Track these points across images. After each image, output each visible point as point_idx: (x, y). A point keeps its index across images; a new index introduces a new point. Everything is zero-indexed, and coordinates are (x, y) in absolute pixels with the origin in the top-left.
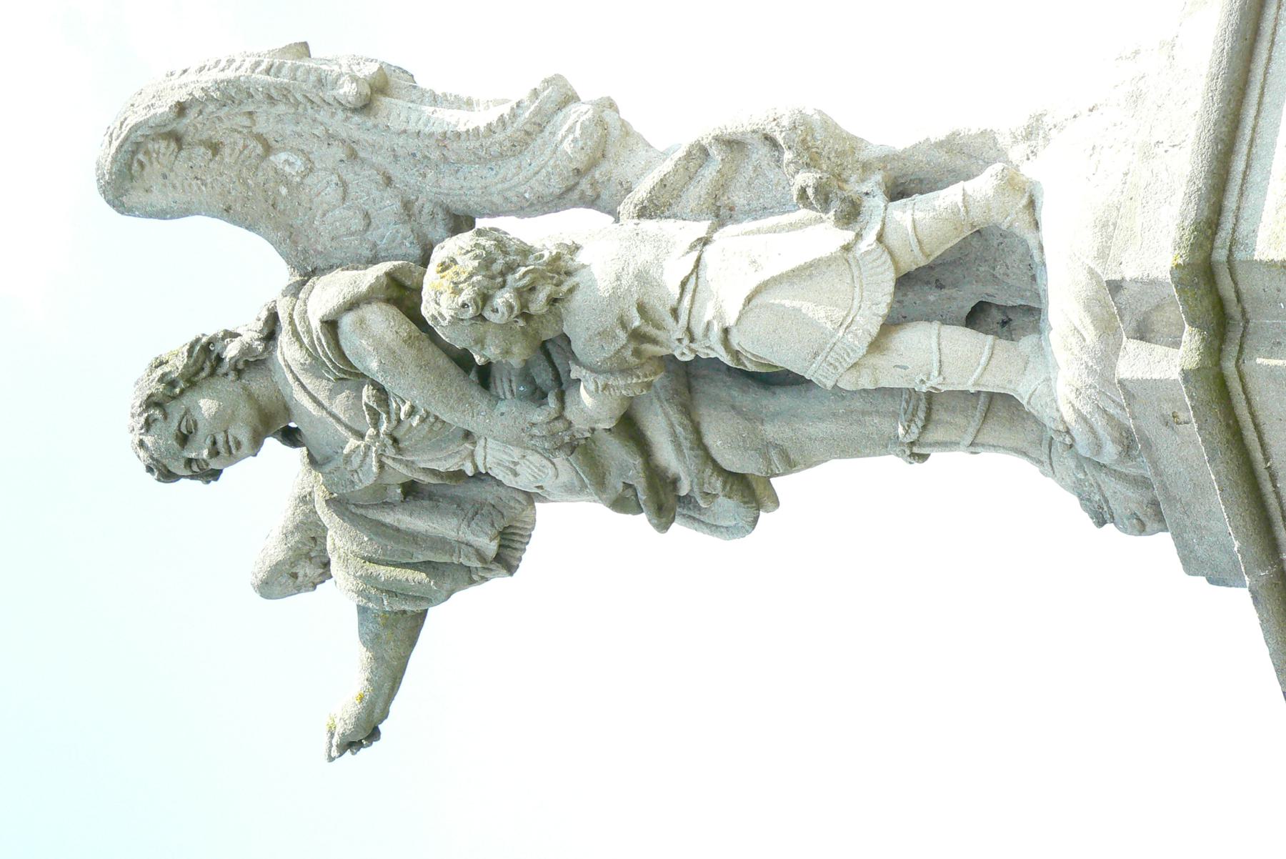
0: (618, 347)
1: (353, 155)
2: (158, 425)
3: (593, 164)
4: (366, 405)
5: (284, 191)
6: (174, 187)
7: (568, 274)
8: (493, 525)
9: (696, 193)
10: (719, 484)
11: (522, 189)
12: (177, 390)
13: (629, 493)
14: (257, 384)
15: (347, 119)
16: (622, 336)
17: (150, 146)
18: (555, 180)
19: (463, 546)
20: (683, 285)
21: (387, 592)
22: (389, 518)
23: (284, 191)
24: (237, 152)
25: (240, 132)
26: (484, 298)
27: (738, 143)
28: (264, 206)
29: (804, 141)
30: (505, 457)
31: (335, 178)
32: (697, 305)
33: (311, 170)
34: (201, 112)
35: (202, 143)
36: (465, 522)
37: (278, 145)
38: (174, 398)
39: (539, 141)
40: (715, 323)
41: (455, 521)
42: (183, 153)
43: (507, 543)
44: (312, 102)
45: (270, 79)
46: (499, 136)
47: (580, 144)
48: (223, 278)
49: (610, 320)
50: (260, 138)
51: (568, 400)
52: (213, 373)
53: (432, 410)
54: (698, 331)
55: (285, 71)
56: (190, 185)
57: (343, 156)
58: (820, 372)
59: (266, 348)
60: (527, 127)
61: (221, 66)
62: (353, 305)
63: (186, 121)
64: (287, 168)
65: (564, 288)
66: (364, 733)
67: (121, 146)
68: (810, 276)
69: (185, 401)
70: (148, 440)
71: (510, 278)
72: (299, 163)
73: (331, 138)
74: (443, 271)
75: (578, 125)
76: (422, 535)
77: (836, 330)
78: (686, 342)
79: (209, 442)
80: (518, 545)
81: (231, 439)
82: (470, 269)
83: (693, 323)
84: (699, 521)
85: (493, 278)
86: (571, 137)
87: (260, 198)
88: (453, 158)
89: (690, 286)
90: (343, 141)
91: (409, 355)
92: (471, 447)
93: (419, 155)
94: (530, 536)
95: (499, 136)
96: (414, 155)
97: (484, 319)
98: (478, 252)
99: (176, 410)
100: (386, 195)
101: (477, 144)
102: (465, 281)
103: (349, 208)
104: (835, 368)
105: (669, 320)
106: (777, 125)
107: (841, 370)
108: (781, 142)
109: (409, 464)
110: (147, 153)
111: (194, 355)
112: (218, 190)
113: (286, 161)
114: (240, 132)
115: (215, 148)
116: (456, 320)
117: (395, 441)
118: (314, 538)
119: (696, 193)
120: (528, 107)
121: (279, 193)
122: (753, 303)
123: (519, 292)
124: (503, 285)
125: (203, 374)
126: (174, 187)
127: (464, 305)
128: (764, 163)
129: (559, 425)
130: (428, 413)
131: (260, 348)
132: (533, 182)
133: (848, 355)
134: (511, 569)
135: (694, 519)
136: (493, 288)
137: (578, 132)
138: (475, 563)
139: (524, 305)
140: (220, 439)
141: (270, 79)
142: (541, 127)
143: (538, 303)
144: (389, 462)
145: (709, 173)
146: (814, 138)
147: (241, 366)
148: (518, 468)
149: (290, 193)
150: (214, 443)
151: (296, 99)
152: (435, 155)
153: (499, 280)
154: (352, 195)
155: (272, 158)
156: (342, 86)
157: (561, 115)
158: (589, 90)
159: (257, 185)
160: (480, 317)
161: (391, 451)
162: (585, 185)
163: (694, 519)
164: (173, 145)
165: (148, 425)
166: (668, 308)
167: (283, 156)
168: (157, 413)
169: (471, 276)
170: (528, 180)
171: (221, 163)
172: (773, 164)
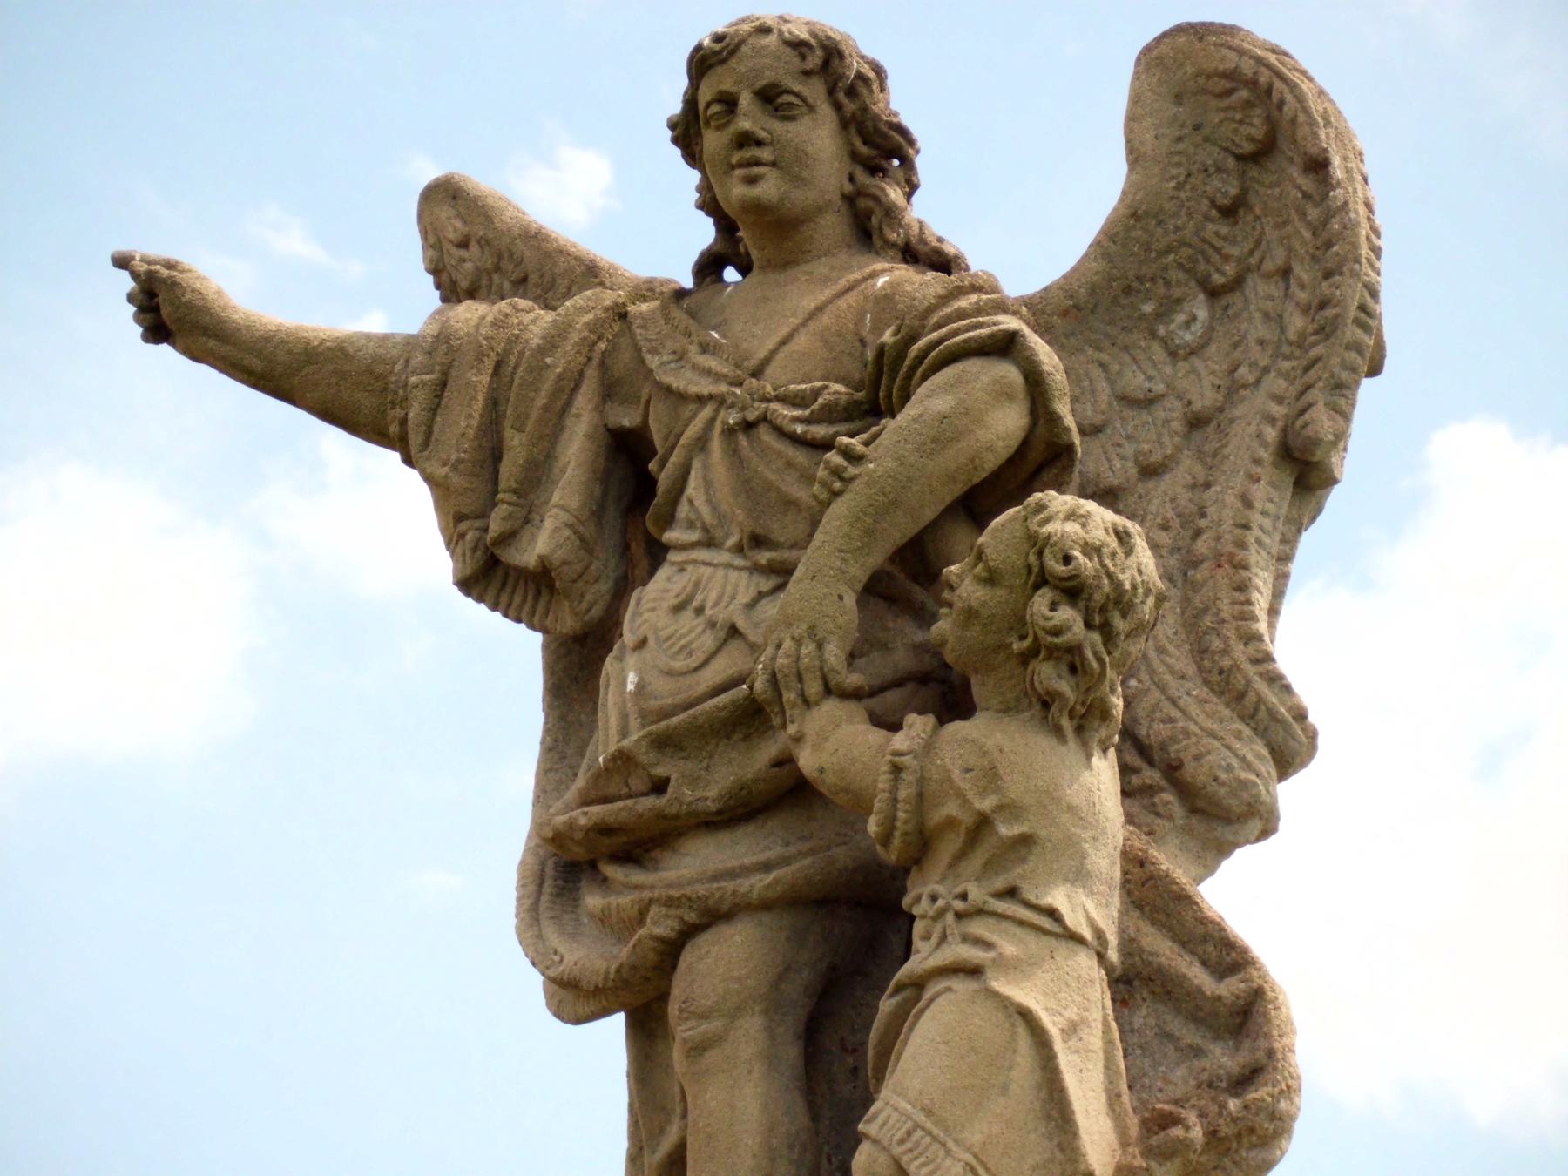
0: (970, 795)
1: (1196, 422)
2: (796, 60)
3: (1186, 792)
4: (826, 387)
5: (1148, 308)
6: (1179, 139)
7: (1079, 730)
8: (564, 563)
9: (1161, 948)
10: (659, 931)
11: (1144, 676)
12: (841, 96)
13: (637, 784)
14: (833, 225)
15: (1272, 420)
16: (986, 804)
17: (1258, 111)
18: (1163, 730)
19: (524, 512)
20: (1052, 913)
21: (443, 385)
22: (584, 402)
23: (1148, 308)
24: (1218, 243)
25: (1251, 252)
26: (1072, 591)
27: (1242, 1025)
28: (1131, 274)
29: (1252, 1130)
30: (713, 595)
31: (1160, 388)
32: (1018, 931)
33: (1173, 354)
34: (1306, 196)
35: (1244, 192)
36: (572, 520)
37: (1219, 312)
38: (831, 92)
39: (1227, 712)
40: (991, 954)
41: (574, 503)
42: (1231, 162)
43: (511, 581)
44: (1307, 369)
45: (1352, 311)
46: (1239, 651)
47: (1223, 776)
48: (1021, 188)
49: (1015, 788)
50: (1237, 283)
51: (852, 706)
52: (854, 156)
53: (856, 485)
54: (978, 927)
55: (1359, 333)
56: (1178, 165)
57: (1197, 406)
58: (895, 1116)
59: (894, 245)
60: (1251, 698)
61: (1373, 237)
62: (1035, 382)
63: (1295, 172)
64: (1181, 318)
65: (1065, 723)
66: (168, 310)
67: (1268, 66)
68: (1048, 1117)
69: (825, 110)
70: (771, 40)
71: (1096, 637)
72: (1188, 337)
73: (1233, 390)
74: (1117, 533)
75: (1253, 777)
76: (545, 443)
77: (968, 1149)
78: (959, 905)
79: (762, 134)
80: (504, 598)
81: (762, 170)
82: (1121, 577)
83: (992, 921)
84: (539, 893)
85: (1103, 610)
86: (1235, 762)
87: (1144, 270)
88: (1198, 575)
89: (1046, 923)
90: (1221, 410)
91: (950, 459)
92: (731, 542)
93: (1203, 523)
94: (518, 620)
95: (1239, 651)
96: (1203, 515)
97: (1036, 587)
98: (1140, 591)
99: (815, 90)
100: (1130, 464)
101: (1225, 615)
102: (1104, 566)
103: (1110, 404)
104: (902, 1141)
105: (1000, 883)
106: (1282, 1091)
107: (897, 1150)
108: (1251, 1096)
109: (702, 443)
110: (1248, 104)
111: (892, 133)
112: (1167, 206)
113: (1194, 318)
114: (1251, 252)
115: (1229, 212)
116: (1039, 544)
117: (748, 426)
118: (524, 280)
119: (1161, 948)
120: (1283, 703)
121: (1148, 299)
122: (1019, 1022)
123: (1074, 650)
124: (1088, 625)
125: (858, 143)
126: (1179, 139)
127: (1067, 559)
128: (1205, 1063)
129: (814, 688)
130: (852, 479)
131: (893, 237)
132: (1156, 694)
133: (924, 1165)
134: (468, 585)
135: (541, 885)
136: (1087, 608)
137: (1244, 775)
138: (495, 526)
139: (1053, 653)
140: (765, 154)
141: (1352, 311)
142: (1249, 717)
143: (1048, 675)
144: (707, 411)
145: (1198, 976)
146: (1254, 1146)
147: (863, 203)
148: (688, 614)
149: (1143, 316)
150: (759, 143)
151: (1313, 345)
152: (1202, 546)
153: (1097, 620)
154: (1128, 413)
155: (1201, 297)
156: (1330, 418)
157: (1265, 752)
158: (1290, 795)
159: (1165, 269)
160: (1042, 579)
161: (732, 418)
162: (1151, 776)
163: (541, 885)
164: (1248, 148)
165: (798, 46)
166: (1019, 883)
167: (1202, 314)
168: (814, 61)
169: (1110, 576)
170: (1163, 688)
171: (1207, 218)
172: (1205, 1076)
